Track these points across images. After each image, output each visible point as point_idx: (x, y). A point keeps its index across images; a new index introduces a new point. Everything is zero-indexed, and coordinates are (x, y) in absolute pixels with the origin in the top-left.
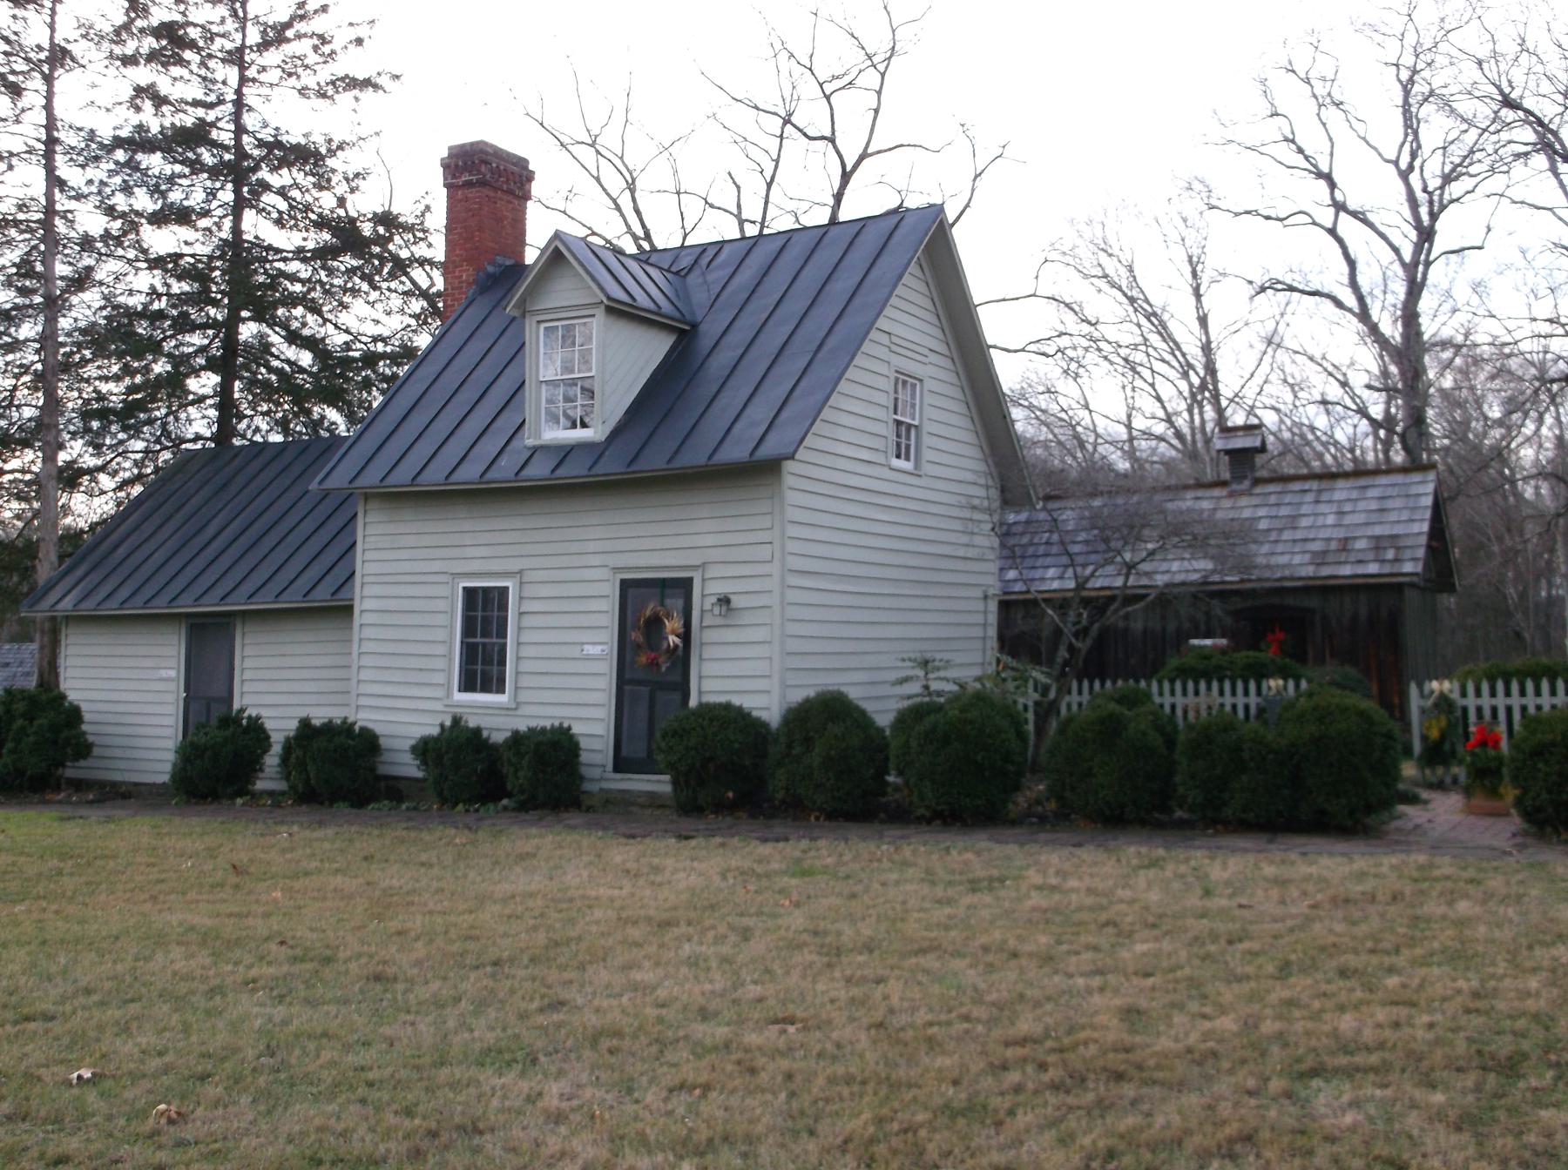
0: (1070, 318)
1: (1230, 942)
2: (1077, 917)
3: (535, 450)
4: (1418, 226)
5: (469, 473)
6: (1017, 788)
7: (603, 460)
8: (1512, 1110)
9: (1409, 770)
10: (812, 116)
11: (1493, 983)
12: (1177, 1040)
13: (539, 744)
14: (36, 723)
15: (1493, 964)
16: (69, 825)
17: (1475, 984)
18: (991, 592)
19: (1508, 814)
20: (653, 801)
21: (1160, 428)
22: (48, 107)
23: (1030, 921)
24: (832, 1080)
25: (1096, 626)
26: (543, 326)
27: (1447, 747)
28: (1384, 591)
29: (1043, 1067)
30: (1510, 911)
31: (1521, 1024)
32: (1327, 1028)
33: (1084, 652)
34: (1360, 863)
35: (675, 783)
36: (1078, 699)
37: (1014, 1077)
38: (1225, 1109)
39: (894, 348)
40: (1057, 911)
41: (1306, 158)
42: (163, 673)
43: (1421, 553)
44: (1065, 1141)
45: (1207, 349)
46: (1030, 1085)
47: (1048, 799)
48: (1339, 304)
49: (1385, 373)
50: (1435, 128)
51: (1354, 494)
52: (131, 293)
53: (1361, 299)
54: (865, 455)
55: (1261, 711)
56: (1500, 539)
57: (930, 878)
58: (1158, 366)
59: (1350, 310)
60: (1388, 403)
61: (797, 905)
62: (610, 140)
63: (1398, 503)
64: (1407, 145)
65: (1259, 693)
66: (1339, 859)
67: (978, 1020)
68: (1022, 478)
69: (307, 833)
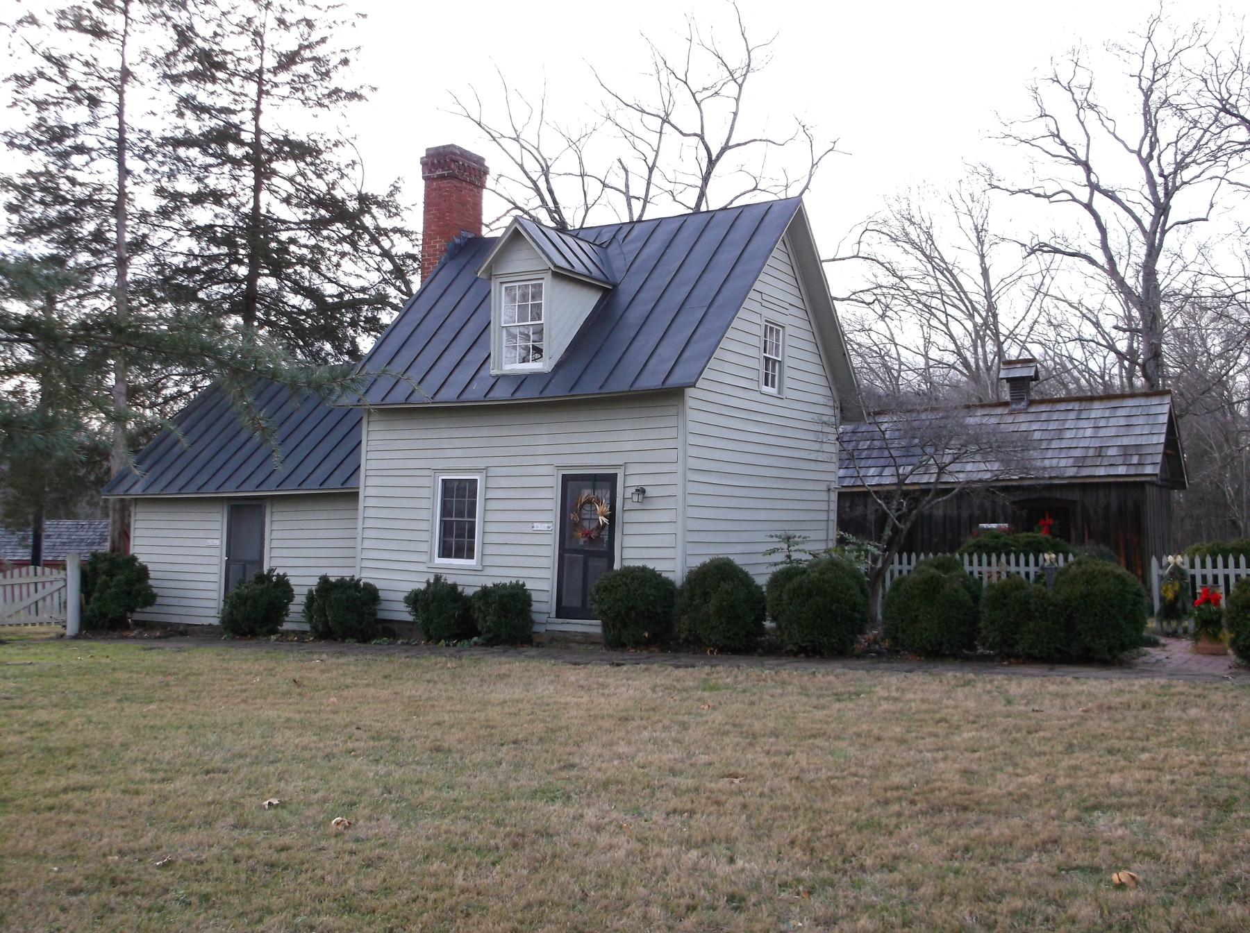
0: (880, 271)
1: (1029, 733)
2: (917, 717)
3: (498, 378)
4: (1156, 203)
5: (449, 394)
6: (862, 632)
7: (550, 386)
8: (1227, 830)
9: (1152, 624)
10: (685, 116)
11: (1214, 758)
12: (1000, 788)
13: (502, 597)
14: (115, 579)
15: (1215, 746)
16: (153, 653)
17: (1202, 758)
18: (833, 486)
19: (1225, 654)
20: (587, 639)
21: (951, 358)
22: (120, 114)
23: (885, 718)
24: (774, 808)
25: (914, 512)
26: (505, 285)
27: (1179, 605)
28: (1130, 488)
29: (913, 802)
30: (1227, 715)
31: (1233, 781)
32: (1102, 782)
33: (905, 532)
34: (1117, 684)
35: (605, 625)
36: (903, 567)
37: (895, 808)
38: (1038, 826)
39: (765, 303)
40: (901, 712)
41: (1068, 149)
42: (210, 542)
43: (1159, 459)
44: (938, 841)
45: (988, 295)
46: (907, 813)
47: (883, 640)
48: (1092, 262)
49: (1129, 318)
50: (1169, 126)
51: (1107, 414)
52: (175, 254)
53: (1111, 259)
54: (743, 383)
55: (1038, 577)
56: (1220, 447)
57: (804, 692)
58: (951, 310)
59: (1102, 268)
60: (1131, 340)
61: (714, 708)
62: (529, 136)
63: (1141, 420)
64: (1147, 140)
65: (1037, 564)
66: (1102, 681)
67: (863, 777)
68: (855, 398)
69: (334, 660)
